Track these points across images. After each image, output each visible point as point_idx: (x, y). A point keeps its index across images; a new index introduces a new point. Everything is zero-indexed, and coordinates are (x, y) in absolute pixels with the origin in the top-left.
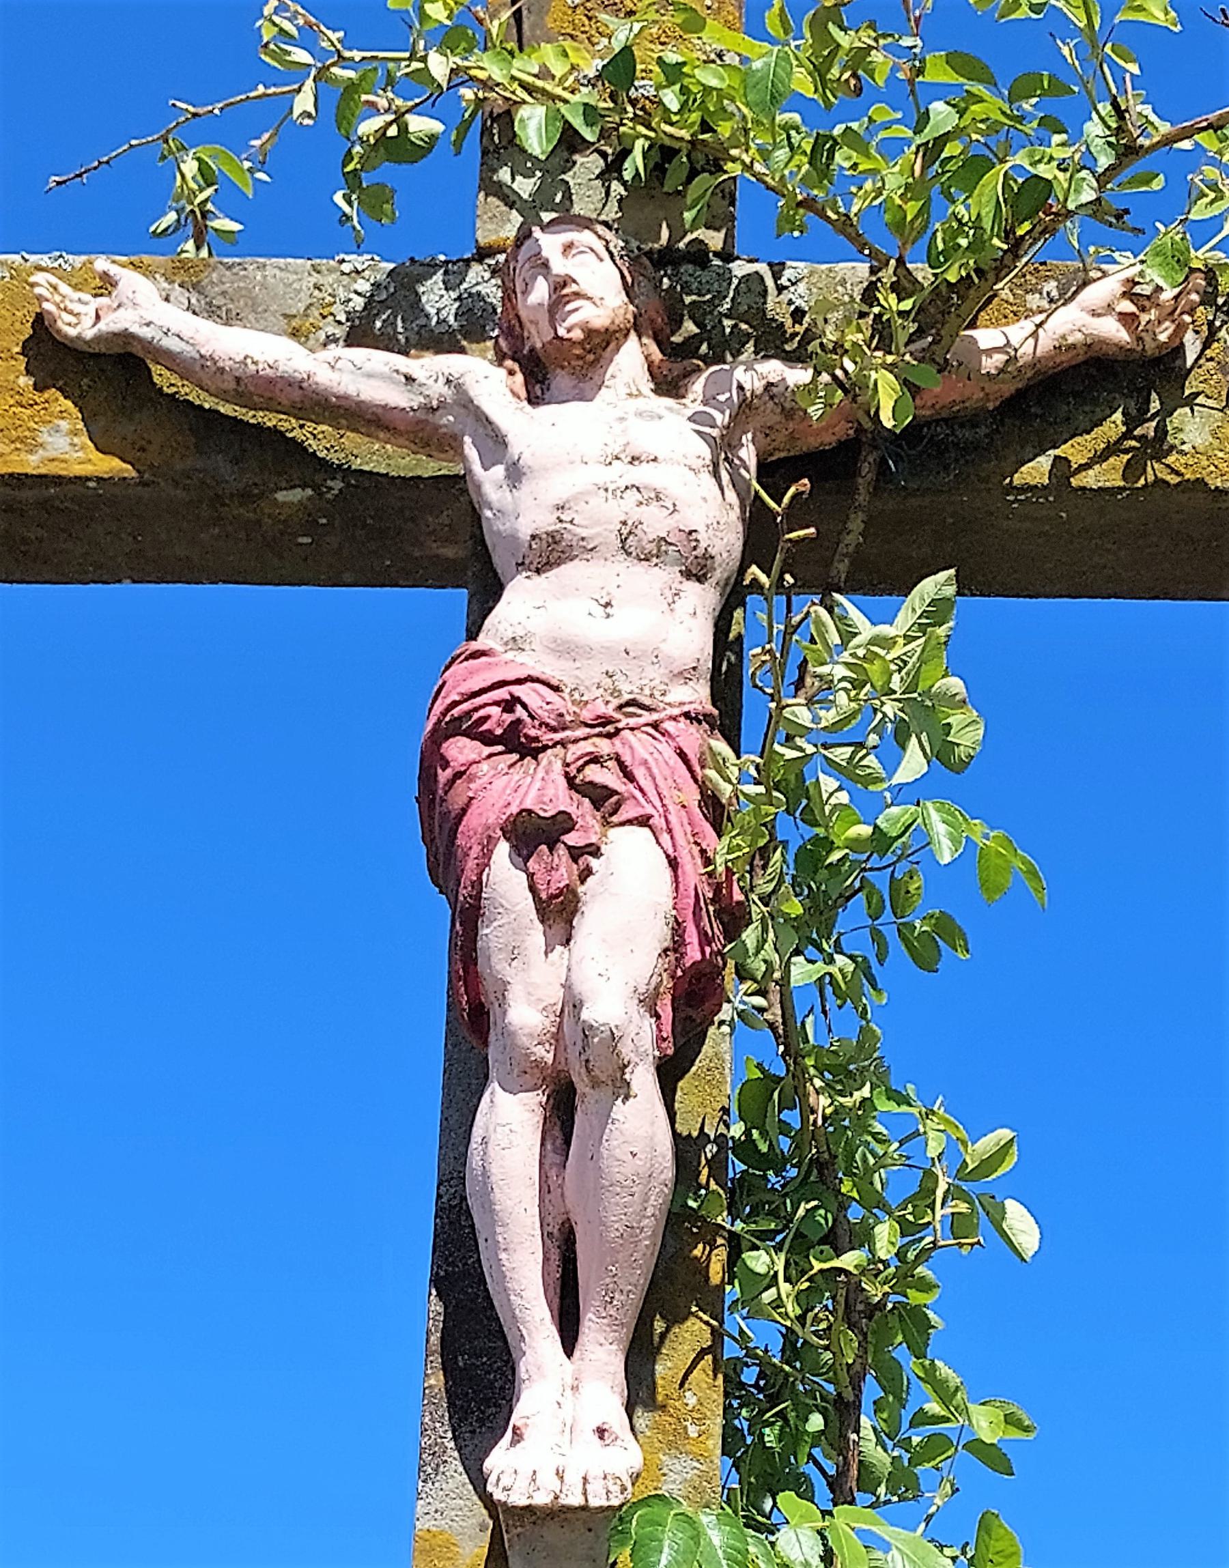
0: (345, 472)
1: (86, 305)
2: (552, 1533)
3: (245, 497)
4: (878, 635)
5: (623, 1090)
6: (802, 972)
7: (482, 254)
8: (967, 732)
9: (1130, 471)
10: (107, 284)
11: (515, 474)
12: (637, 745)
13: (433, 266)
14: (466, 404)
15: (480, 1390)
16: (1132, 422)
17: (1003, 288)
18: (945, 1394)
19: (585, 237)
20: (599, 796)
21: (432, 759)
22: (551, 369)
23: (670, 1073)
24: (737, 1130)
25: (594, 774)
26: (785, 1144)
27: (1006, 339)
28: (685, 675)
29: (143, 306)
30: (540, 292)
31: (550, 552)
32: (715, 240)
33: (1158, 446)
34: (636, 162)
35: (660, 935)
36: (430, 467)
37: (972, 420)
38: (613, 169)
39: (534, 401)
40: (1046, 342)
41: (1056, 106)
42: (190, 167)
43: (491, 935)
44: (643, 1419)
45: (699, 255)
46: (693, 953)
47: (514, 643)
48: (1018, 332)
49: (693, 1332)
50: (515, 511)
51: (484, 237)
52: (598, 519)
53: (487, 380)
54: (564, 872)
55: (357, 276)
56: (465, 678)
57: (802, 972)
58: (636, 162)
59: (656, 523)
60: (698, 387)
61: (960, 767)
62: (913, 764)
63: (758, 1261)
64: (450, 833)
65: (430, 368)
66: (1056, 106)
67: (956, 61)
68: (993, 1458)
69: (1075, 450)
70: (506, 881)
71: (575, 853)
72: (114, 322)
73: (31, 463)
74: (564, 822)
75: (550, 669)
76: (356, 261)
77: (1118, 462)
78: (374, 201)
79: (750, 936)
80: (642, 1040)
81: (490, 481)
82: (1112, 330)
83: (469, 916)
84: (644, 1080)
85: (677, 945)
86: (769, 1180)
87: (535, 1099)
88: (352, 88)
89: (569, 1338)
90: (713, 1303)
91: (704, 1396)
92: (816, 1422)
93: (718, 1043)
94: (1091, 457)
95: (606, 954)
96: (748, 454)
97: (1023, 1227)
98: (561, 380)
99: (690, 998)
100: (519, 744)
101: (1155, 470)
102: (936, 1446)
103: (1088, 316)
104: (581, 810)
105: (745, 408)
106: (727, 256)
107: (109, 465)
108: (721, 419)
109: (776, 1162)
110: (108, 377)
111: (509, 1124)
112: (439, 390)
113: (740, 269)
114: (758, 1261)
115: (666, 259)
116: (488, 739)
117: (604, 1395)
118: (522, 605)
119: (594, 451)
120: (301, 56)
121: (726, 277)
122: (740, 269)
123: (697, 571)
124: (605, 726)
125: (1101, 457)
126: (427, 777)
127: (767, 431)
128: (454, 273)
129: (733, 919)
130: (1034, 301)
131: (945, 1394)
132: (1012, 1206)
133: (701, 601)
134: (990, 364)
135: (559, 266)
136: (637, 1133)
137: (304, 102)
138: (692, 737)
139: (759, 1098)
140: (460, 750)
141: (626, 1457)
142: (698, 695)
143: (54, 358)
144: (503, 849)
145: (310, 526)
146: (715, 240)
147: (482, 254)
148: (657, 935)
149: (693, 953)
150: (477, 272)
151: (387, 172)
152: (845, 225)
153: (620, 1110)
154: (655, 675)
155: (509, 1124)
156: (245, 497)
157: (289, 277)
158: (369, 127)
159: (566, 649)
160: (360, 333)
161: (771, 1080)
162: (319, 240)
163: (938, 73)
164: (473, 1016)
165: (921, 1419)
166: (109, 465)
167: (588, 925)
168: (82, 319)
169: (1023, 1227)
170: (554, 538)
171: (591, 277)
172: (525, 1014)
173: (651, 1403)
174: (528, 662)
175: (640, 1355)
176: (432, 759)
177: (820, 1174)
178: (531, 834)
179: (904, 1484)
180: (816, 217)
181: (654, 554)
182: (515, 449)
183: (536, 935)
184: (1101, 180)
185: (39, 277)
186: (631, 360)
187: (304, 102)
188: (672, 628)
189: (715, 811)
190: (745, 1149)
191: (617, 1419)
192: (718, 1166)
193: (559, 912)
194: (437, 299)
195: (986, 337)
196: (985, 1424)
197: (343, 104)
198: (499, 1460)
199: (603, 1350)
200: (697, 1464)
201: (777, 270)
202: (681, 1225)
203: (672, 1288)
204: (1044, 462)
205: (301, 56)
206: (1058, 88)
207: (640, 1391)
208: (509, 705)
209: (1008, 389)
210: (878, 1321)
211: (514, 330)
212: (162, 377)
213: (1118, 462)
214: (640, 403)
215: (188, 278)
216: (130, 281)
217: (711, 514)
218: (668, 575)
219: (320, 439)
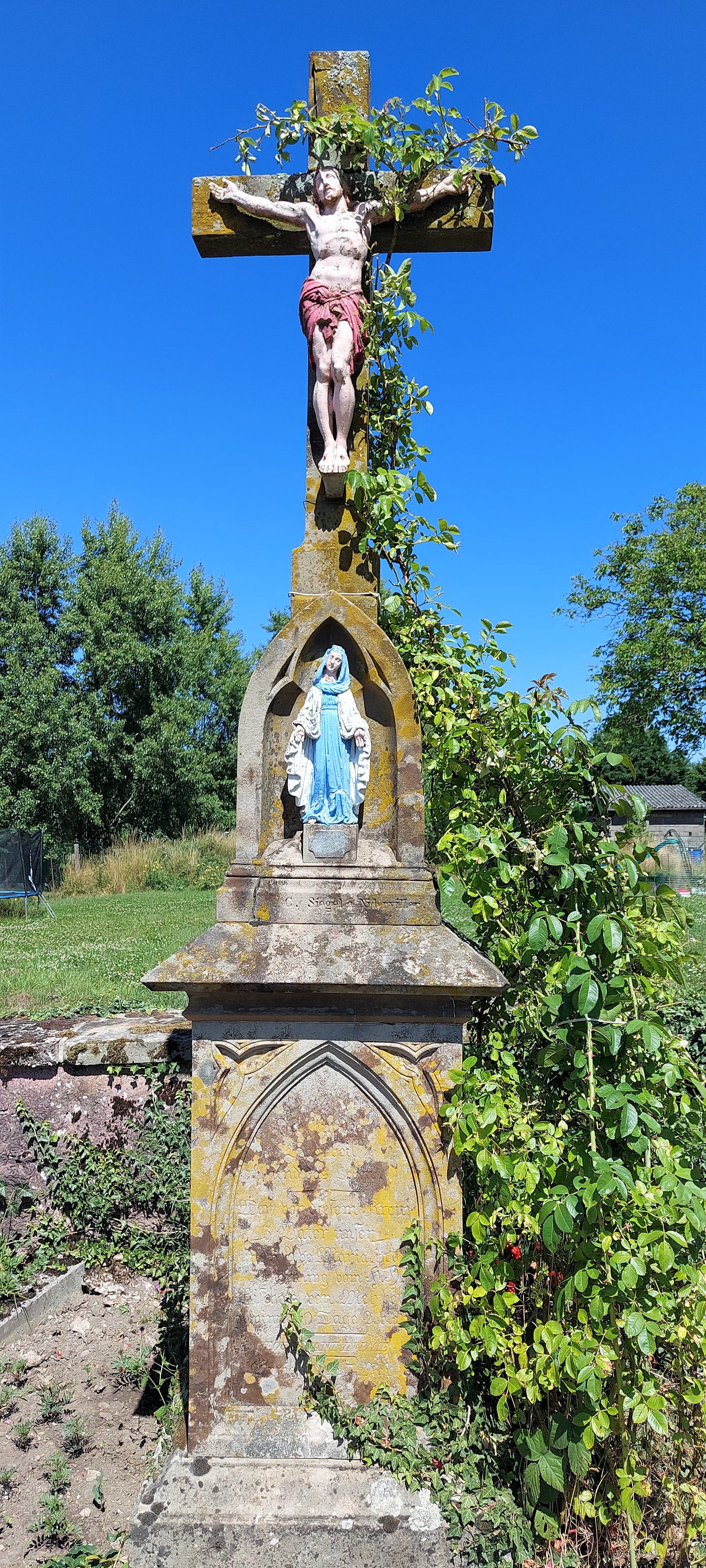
0: (281, 231)
1: (222, 190)
2: (332, 478)
3: (259, 237)
4: (396, 272)
5: (343, 382)
6: (382, 351)
7: (310, 172)
8: (413, 299)
9: (456, 224)
10: (225, 185)
11: (317, 235)
12: (345, 301)
13: (298, 176)
14: (306, 215)
15: (318, 449)
16: (456, 211)
17: (428, 177)
18: (413, 445)
19: (331, 172)
20: (337, 314)
21: (302, 306)
22: (325, 206)
23: (354, 378)
24: (370, 387)
25: (336, 309)
26: (380, 390)
27: (426, 192)
28: (355, 283)
29: (234, 191)
30: (321, 187)
31: (325, 254)
32: (362, 166)
33: (462, 217)
34: (344, 147)
35: (350, 346)
36: (299, 230)
37: (420, 212)
38: (339, 148)
39: (321, 214)
40: (436, 193)
41: (435, 136)
42: (242, 143)
43: (315, 347)
44: (351, 453)
45: (359, 170)
46: (357, 351)
47: (318, 277)
48: (429, 190)
49: (361, 433)
50: (319, 244)
51: (310, 168)
52: (335, 246)
53: (311, 209)
54: (330, 333)
55: (282, 178)
56: (308, 286)
57: (382, 351)
58: (344, 147)
59: (348, 247)
60: (358, 209)
61: (412, 306)
62: (402, 306)
63: (374, 417)
64: (307, 317)
65: (299, 206)
66: (435, 136)
67: (412, 126)
68: (423, 458)
69: (443, 219)
70: (318, 334)
71: (332, 328)
72: (229, 195)
73: (212, 232)
74: (330, 321)
75: (326, 283)
76: (281, 175)
77: (453, 221)
78: (285, 156)
79: (369, 346)
80: (347, 370)
81: (312, 234)
82: (451, 188)
83: (311, 343)
84: (348, 380)
85: (354, 349)
86: (378, 399)
87: (326, 384)
88: (279, 127)
89: (335, 438)
90: (365, 427)
91: (362, 448)
92: (387, 452)
93: (365, 369)
94: (446, 221)
95: (337, 354)
96: (369, 225)
97: (430, 407)
98: (327, 209)
99: (357, 361)
100: (320, 302)
101: (461, 223)
102: (412, 456)
103: (446, 185)
104: (333, 317)
105: (368, 214)
106: (365, 170)
107: (229, 231)
108: (362, 217)
109: (378, 395)
110: (227, 209)
111: (321, 389)
112: (300, 212)
113: (368, 173)
114: (374, 417)
115: (352, 171)
116: (313, 301)
117: (342, 449)
118: (320, 267)
119: (334, 229)
120: (266, 118)
121: (365, 175)
122: (368, 173)
123: (357, 258)
124: (338, 297)
125: (449, 221)
126: (301, 310)
127: (374, 219)
128: (303, 177)
129: (366, 341)
130: (435, 180)
131: (413, 445)
132: (428, 403)
133: (358, 264)
134: (423, 199)
135: (326, 181)
136: (347, 391)
137: (268, 131)
138: (356, 298)
139: (376, 380)
140: (308, 304)
141: (347, 462)
142: (358, 288)
143: (216, 205)
144: (317, 327)
145: (274, 243)
146: (362, 166)
147: (310, 172)
148: (350, 346)
149: (357, 351)
150: (309, 177)
151: (289, 148)
152: (390, 165)
153: (343, 387)
154: (349, 284)
155: (321, 389)
156: (259, 237)
157: (266, 180)
158: (283, 136)
159: (329, 278)
160: (284, 197)
161: (377, 376)
162: (273, 169)
163: (409, 129)
164: (313, 365)
165: (409, 450)
166: (229, 231)
167: (336, 344)
168: (221, 194)
169: (430, 407)
170: (326, 251)
171: (332, 182)
172: (323, 366)
173: (353, 450)
174: (322, 282)
175: (350, 440)
176: (302, 306)
177: (387, 399)
178: (323, 324)
179: (406, 463)
180: (383, 161)
181: (348, 254)
182: (317, 228)
183: (325, 347)
184: (446, 155)
185: (211, 184)
186: (343, 203)
187: (268, 131)
188: (352, 271)
189: (362, 316)
190: (371, 392)
191: (345, 454)
192: (366, 397)
193: (329, 341)
194: (300, 185)
195: (422, 192)
196: (421, 451)
197: (277, 131)
198: (322, 463)
199: (342, 440)
200: (361, 462)
201: (376, 173)
202: (357, 411)
203: (357, 424)
204: (436, 222)
205: (266, 118)
206: (435, 132)
207: (350, 448)
208: (317, 293)
209: (427, 205)
210: (399, 431)
211: (316, 196)
212: (239, 208)
213: (453, 221)
214: (344, 215)
215: (243, 180)
216: (231, 184)
217: (360, 243)
218: (351, 259)
219: (275, 224)
